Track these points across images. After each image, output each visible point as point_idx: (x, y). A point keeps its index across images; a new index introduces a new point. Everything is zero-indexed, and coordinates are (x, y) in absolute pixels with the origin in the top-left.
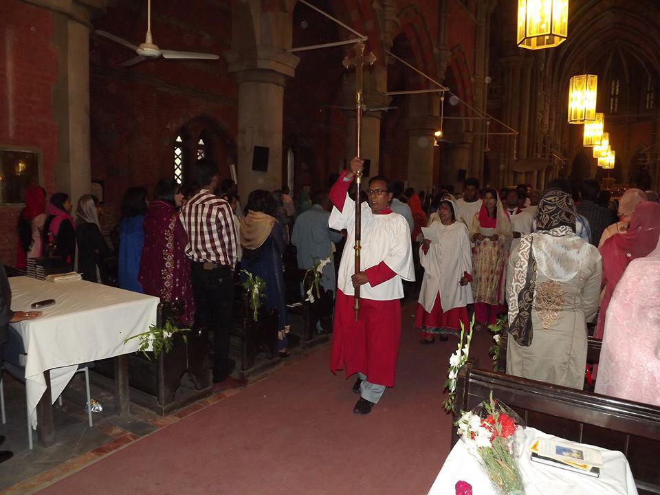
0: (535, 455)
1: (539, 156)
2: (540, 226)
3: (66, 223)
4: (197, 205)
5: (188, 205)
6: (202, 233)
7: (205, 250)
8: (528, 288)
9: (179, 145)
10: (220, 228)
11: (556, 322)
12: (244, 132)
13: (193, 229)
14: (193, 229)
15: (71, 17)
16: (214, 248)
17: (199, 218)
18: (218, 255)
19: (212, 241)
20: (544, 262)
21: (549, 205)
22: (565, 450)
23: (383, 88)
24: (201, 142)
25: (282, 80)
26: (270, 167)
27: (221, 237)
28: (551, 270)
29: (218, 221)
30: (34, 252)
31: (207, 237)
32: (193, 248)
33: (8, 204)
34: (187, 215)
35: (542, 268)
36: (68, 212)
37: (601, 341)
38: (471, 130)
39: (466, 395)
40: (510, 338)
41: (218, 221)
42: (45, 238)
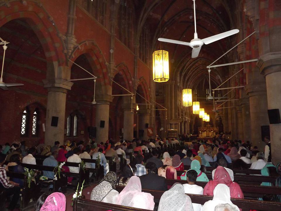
1: (180, 118)
9: (25, 114)
12: (49, 111)
25: (65, 91)
26: (58, 125)
37: (213, 196)
38: (150, 108)
39: (77, 208)
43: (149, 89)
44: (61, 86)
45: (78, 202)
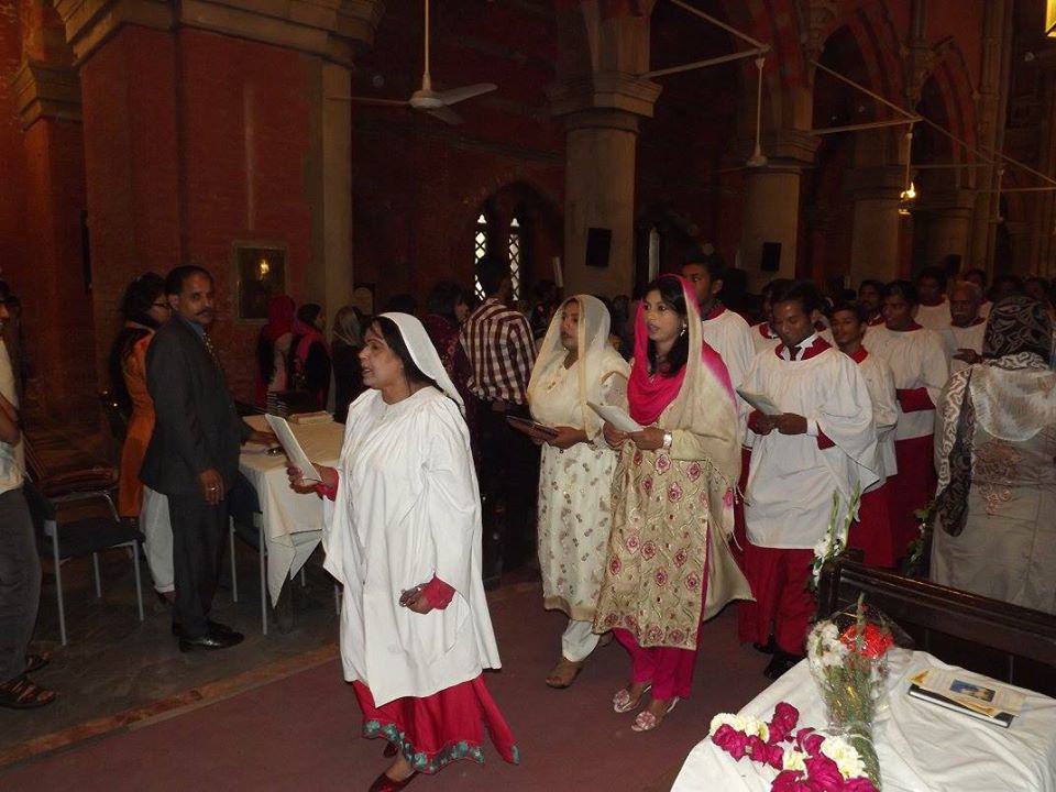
0: (915, 688)
2: (989, 351)
3: (318, 347)
4: (483, 321)
5: (470, 321)
6: (490, 361)
7: (494, 384)
8: (960, 450)
9: (481, 228)
10: (513, 353)
11: (1007, 505)
13: (478, 355)
14: (478, 355)
15: (327, 58)
16: (506, 381)
17: (485, 339)
18: (511, 391)
19: (503, 371)
20: (988, 410)
21: (1004, 318)
22: (967, 687)
23: (804, 121)
24: (515, 223)
25: (632, 123)
27: (515, 365)
28: (998, 427)
29: (510, 342)
30: (277, 383)
31: (496, 366)
32: (478, 382)
33: (247, 320)
34: (469, 335)
35: (984, 422)
36: (320, 331)
38: (972, 184)
40: (937, 525)
41: (510, 342)
42: (290, 367)
43: (976, 96)
44: (617, 106)
45: (842, 579)
